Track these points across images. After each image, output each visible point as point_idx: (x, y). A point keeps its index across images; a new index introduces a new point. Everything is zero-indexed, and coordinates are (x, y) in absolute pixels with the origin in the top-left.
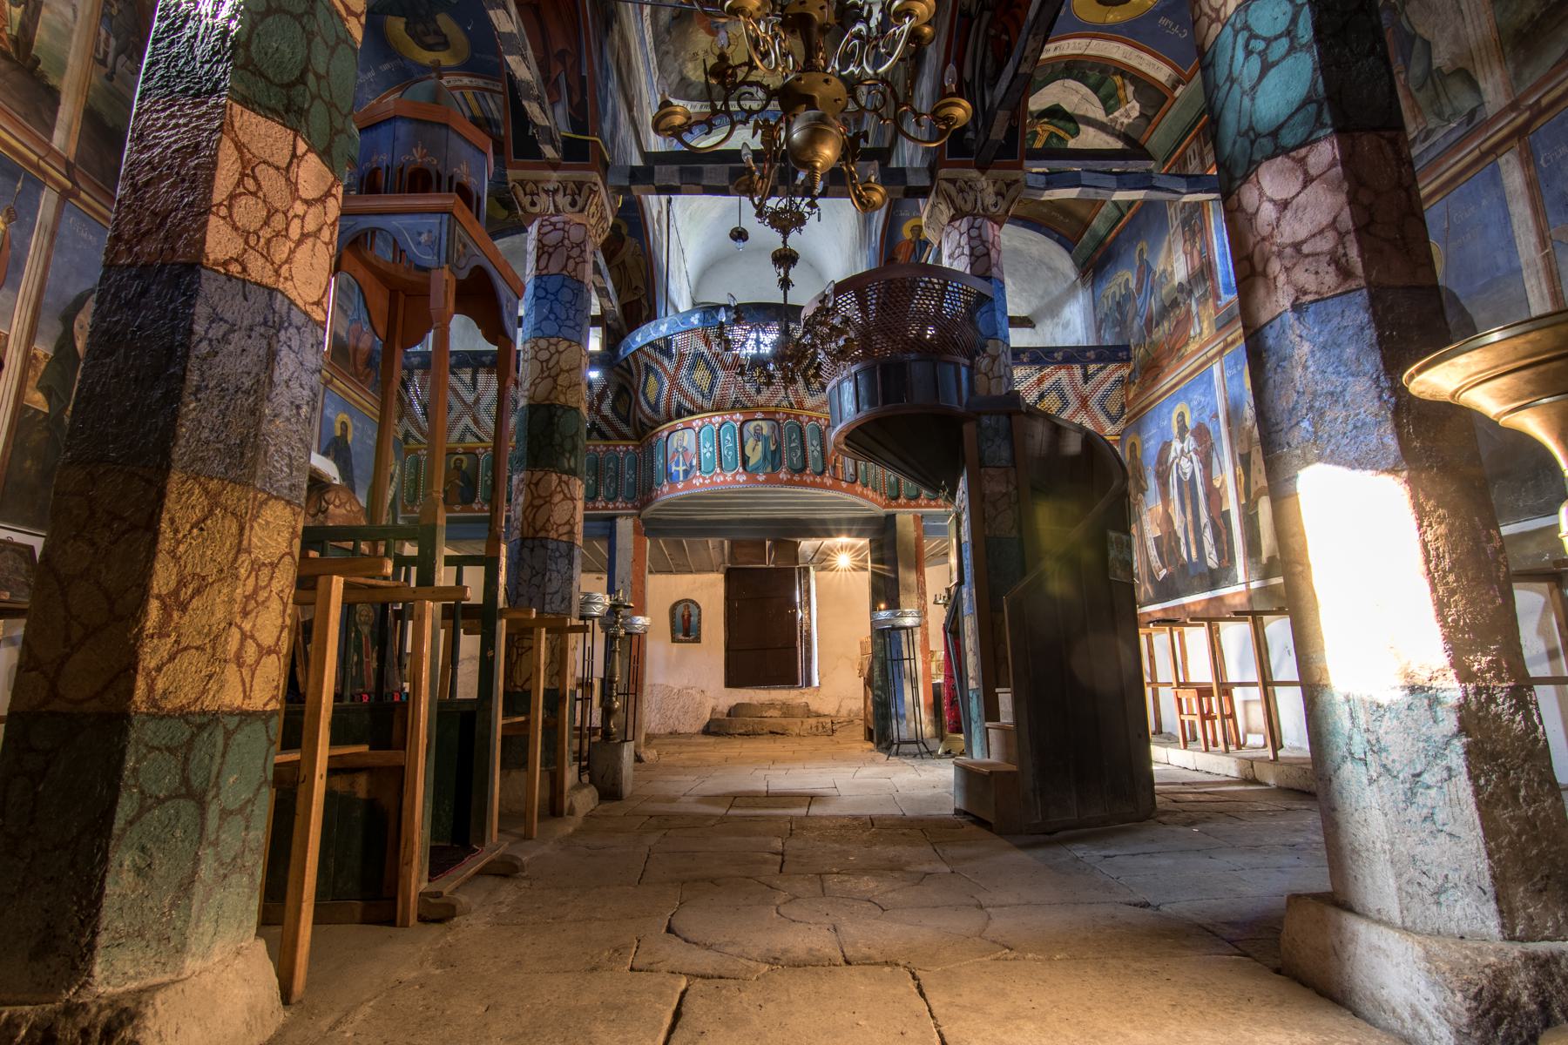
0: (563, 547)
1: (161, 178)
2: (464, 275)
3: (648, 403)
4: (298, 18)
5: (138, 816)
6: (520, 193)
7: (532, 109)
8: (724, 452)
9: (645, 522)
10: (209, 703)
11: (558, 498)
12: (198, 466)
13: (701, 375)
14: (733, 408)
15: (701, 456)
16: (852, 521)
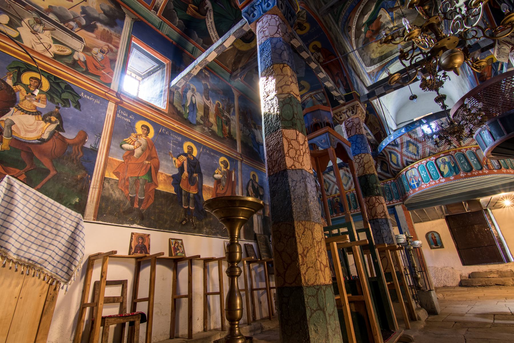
0: (384, 221)
1: (274, 152)
2: (336, 147)
3: (394, 164)
4: (289, 103)
5: (311, 315)
6: (336, 116)
7: (334, 93)
8: (431, 172)
9: (406, 205)
10: (318, 283)
11: (377, 204)
12: (299, 219)
13: (411, 148)
14: (429, 156)
15: (421, 177)
16: (504, 185)
